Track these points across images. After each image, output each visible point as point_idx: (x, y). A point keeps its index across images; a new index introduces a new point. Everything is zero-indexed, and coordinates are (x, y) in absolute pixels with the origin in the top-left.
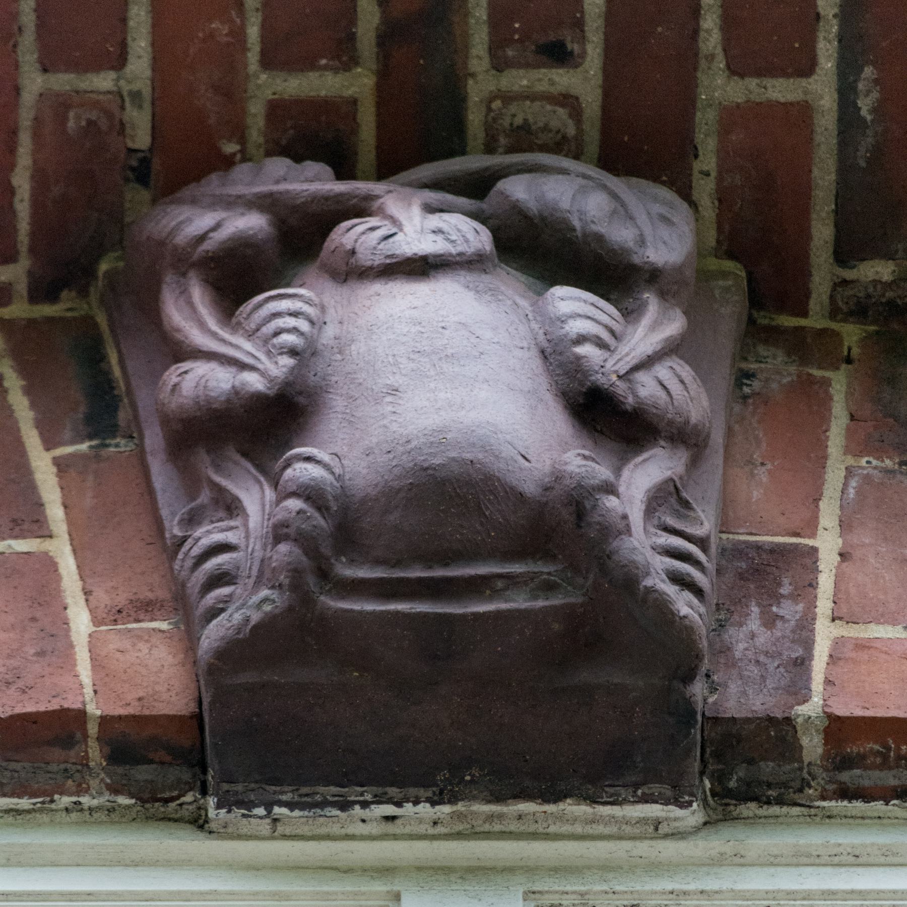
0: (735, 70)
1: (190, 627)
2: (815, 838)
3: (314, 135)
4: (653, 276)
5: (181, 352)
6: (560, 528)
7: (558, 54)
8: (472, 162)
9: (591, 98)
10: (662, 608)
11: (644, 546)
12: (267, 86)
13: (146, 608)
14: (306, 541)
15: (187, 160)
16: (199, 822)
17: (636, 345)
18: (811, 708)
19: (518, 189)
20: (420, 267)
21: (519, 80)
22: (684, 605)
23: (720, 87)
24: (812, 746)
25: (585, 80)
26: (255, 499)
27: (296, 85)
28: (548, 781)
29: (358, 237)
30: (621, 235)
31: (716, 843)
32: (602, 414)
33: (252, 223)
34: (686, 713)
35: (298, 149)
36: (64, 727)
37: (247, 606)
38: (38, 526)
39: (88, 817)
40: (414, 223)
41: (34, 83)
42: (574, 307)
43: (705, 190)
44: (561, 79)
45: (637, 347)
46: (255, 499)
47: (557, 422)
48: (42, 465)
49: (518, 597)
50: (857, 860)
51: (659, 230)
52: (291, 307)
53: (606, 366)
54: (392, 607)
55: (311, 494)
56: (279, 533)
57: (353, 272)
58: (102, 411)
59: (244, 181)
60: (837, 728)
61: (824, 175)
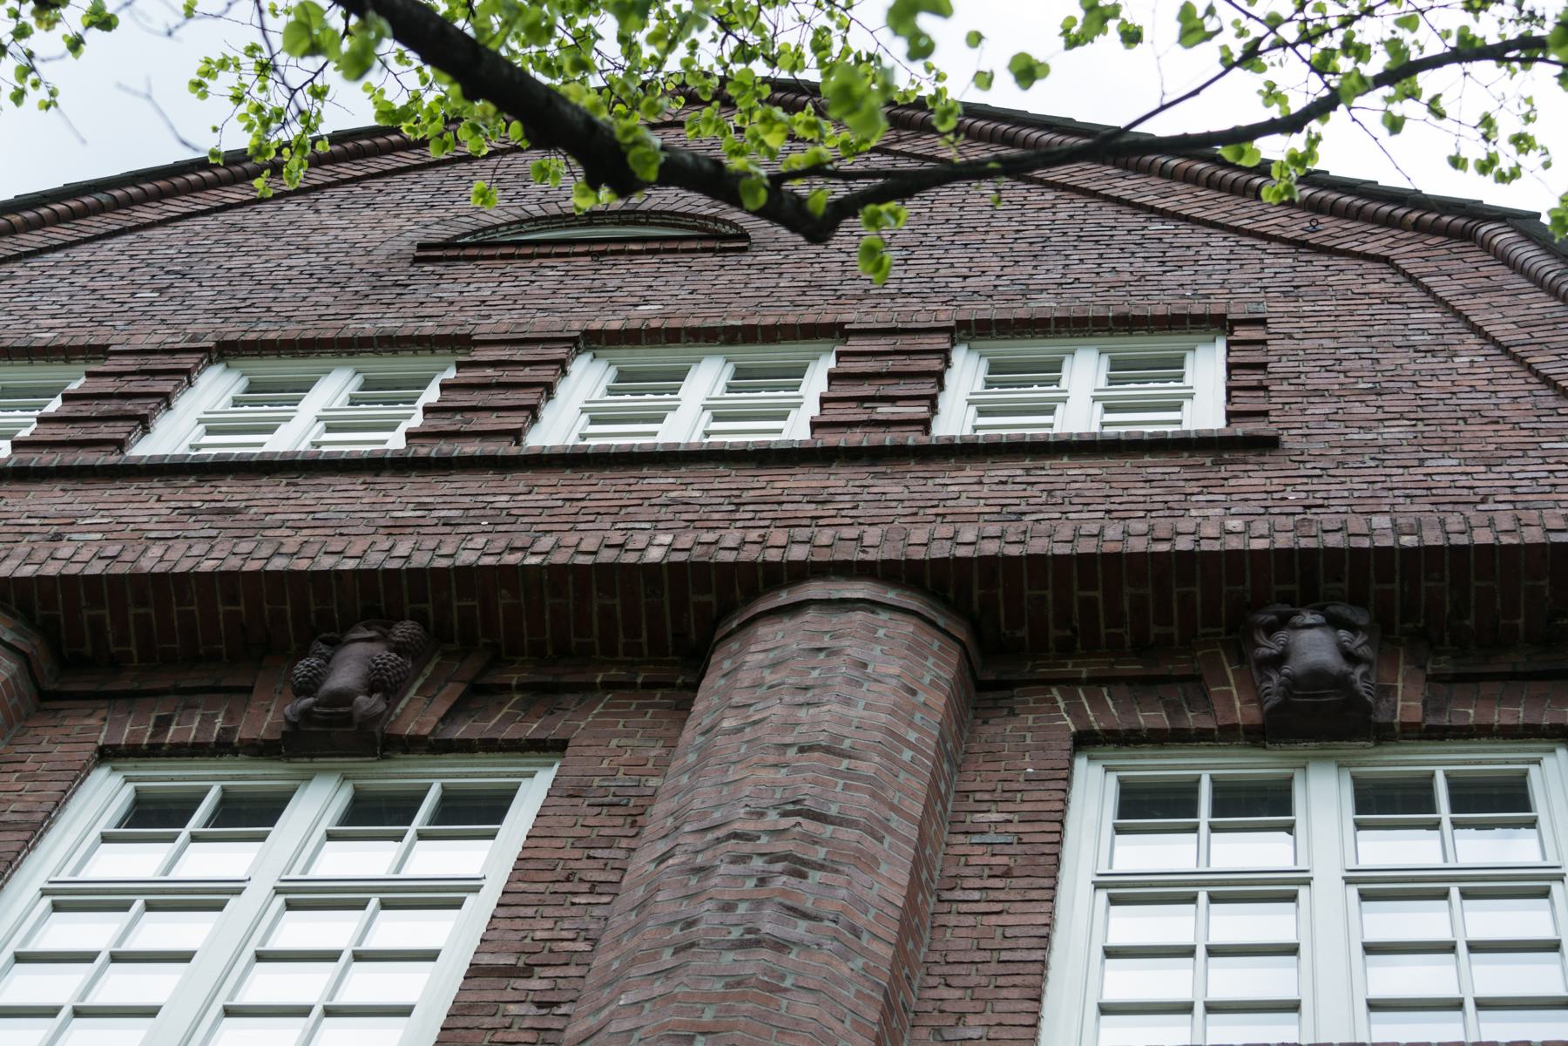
1: (1262, 704)
3: (1287, 599)
4: (1361, 627)
7: (1339, 580)
11: (1360, 686)
13: (1251, 701)
15: (1259, 604)
16: (1264, 747)
17: (1357, 643)
18: (1397, 720)
19: (1331, 609)
20: (1310, 626)
22: (1369, 698)
24: (1397, 729)
25: (1345, 585)
26: (1275, 677)
27: (1281, 588)
29: (1297, 620)
30: (1354, 618)
32: (1350, 657)
33: (1273, 617)
35: (1283, 602)
36: (1234, 727)
37: (1273, 701)
42: (1343, 634)
44: (1341, 585)
45: (1357, 643)
46: (1275, 677)
47: (1340, 659)
48: (1229, 671)
50: (1408, 753)
51: (1363, 619)
52: (1282, 636)
53: (1351, 647)
54: (1175, 606)
55: (1287, 675)
56: (1281, 684)
57: (1296, 628)
58: (1240, 658)
60: (1403, 724)
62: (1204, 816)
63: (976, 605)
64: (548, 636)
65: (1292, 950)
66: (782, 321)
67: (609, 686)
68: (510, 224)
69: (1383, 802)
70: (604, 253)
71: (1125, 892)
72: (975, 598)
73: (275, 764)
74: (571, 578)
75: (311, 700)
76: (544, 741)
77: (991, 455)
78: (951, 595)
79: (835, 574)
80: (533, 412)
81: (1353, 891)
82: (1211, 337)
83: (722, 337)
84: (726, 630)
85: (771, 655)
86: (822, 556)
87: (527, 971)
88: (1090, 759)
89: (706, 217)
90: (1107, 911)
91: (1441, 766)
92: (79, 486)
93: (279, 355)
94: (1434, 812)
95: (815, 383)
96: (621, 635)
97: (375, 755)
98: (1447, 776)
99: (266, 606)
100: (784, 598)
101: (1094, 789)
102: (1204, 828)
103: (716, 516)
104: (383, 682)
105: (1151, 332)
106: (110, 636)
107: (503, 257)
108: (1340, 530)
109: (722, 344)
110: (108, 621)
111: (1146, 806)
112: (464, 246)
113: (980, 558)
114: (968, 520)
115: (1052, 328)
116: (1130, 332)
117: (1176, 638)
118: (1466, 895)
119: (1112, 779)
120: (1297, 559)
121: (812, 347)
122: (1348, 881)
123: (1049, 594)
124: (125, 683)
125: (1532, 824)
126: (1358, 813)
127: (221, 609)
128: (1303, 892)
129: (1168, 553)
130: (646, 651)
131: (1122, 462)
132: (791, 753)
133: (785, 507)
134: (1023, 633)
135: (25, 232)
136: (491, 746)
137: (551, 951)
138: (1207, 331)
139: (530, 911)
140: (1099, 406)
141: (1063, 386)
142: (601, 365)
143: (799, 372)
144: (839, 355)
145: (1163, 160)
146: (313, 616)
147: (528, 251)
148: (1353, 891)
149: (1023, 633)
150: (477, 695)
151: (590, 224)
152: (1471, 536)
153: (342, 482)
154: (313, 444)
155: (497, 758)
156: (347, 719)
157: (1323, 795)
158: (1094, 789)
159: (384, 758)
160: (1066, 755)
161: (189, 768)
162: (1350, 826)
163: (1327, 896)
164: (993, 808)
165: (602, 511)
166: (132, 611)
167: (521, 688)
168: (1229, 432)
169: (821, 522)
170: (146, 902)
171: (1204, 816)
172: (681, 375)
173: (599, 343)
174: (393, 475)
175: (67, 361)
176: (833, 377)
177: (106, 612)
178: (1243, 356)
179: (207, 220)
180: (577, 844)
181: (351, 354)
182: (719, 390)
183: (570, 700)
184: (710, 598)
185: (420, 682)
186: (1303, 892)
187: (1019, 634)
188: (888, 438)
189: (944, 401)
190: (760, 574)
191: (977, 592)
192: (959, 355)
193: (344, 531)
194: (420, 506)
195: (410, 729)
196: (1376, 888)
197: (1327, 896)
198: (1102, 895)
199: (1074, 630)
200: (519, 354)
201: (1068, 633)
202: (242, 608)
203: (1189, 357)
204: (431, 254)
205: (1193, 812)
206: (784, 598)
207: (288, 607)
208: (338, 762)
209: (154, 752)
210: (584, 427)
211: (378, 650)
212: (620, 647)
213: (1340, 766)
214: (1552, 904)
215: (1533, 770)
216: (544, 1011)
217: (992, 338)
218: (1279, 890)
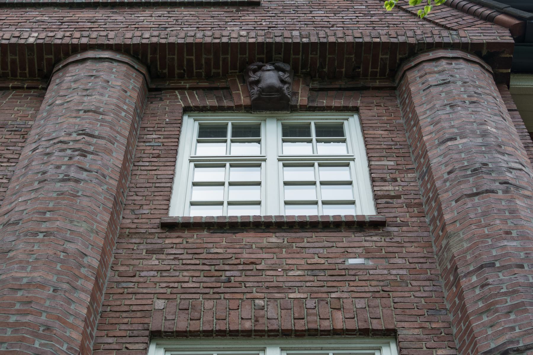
0: (294, 55)
2: (299, 114)
4: (287, 71)
5: (250, 77)
6: (279, 90)
7: (280, 54)
8: (273, 62)
9: (282, 57)
10: (287, 96)
11: (286, 92)
12: (257, 56)
13: (247, 97)
14: (259, 91)
15: (251, 62)
16: (251, 113)
17: (286, 76)
18: (299, 104)
19: (276, 64)
20: (269, 70)
21: (277, 56)
22: (289, 96)
23: (292, 56)
24: (298, 107)
25: (282, 56)
26: (256, 88)
27: (259, 56)
28: (278, 110)
29: (264, 68)
30: (284, 68)
31: (291, 114)
32: (283, 81)
33: (256, 67)
34: (289, 104)
36: (241, 106)
38: (239, 90)
39: (242, 113)
40: (269, 67)
41: (239, 56)
43: (291, 64)
44: (280, 56)
46: (256, 88)
47: (279, 82)
48: (239, 86)
49: (276, 96)
50: (302, 116)
51: (288, 68)
52: (259, 73)
53: (283, 78)
55: (260, 88)
56: (258, 91)
57: (264, 71)
58: (244, 81)
59: (255, 64)
60: (300, 106)
61: (300, 63)
62: (229, 137)
63: (149, 61)
67: (14, 88)
69: (292, 133)
71: (200, 163)
72: (149, 58)
78: (140, 57)
79: (98, 48)
81: (281, 163)
86: (93, 42)
88: (189, 116)
90: (194, 170)
91: (313, 120)
96: (19, 70)
98: (315, 124)
100: (79, 57)
101: (190, 127)
110: (194, 61)
111: (208, 133)
119: (197, 124)
122: (279, 160)
123: (176, 57)
125: (344, 141)
128: (263, 164)
130: (28, 75)
132: (81, 113)
134: (166, 71)
148: (281, 163)
149: (166, 71)
157: (271, 131)
158: (190, 127)
163: (272, 166)
164: (154, 133)
171: (229, 137)
186: (263, 164)
190: (70, 48)
191: (149, 56)
196: (289, 163)
197: (272, 166)
198: (192, 164)
199: (184, 70)
201: (182, 71)
206: (79, 57)
212: (18, 74)
213: (278, 120)
215: (346, 122)
218: (255, 163)
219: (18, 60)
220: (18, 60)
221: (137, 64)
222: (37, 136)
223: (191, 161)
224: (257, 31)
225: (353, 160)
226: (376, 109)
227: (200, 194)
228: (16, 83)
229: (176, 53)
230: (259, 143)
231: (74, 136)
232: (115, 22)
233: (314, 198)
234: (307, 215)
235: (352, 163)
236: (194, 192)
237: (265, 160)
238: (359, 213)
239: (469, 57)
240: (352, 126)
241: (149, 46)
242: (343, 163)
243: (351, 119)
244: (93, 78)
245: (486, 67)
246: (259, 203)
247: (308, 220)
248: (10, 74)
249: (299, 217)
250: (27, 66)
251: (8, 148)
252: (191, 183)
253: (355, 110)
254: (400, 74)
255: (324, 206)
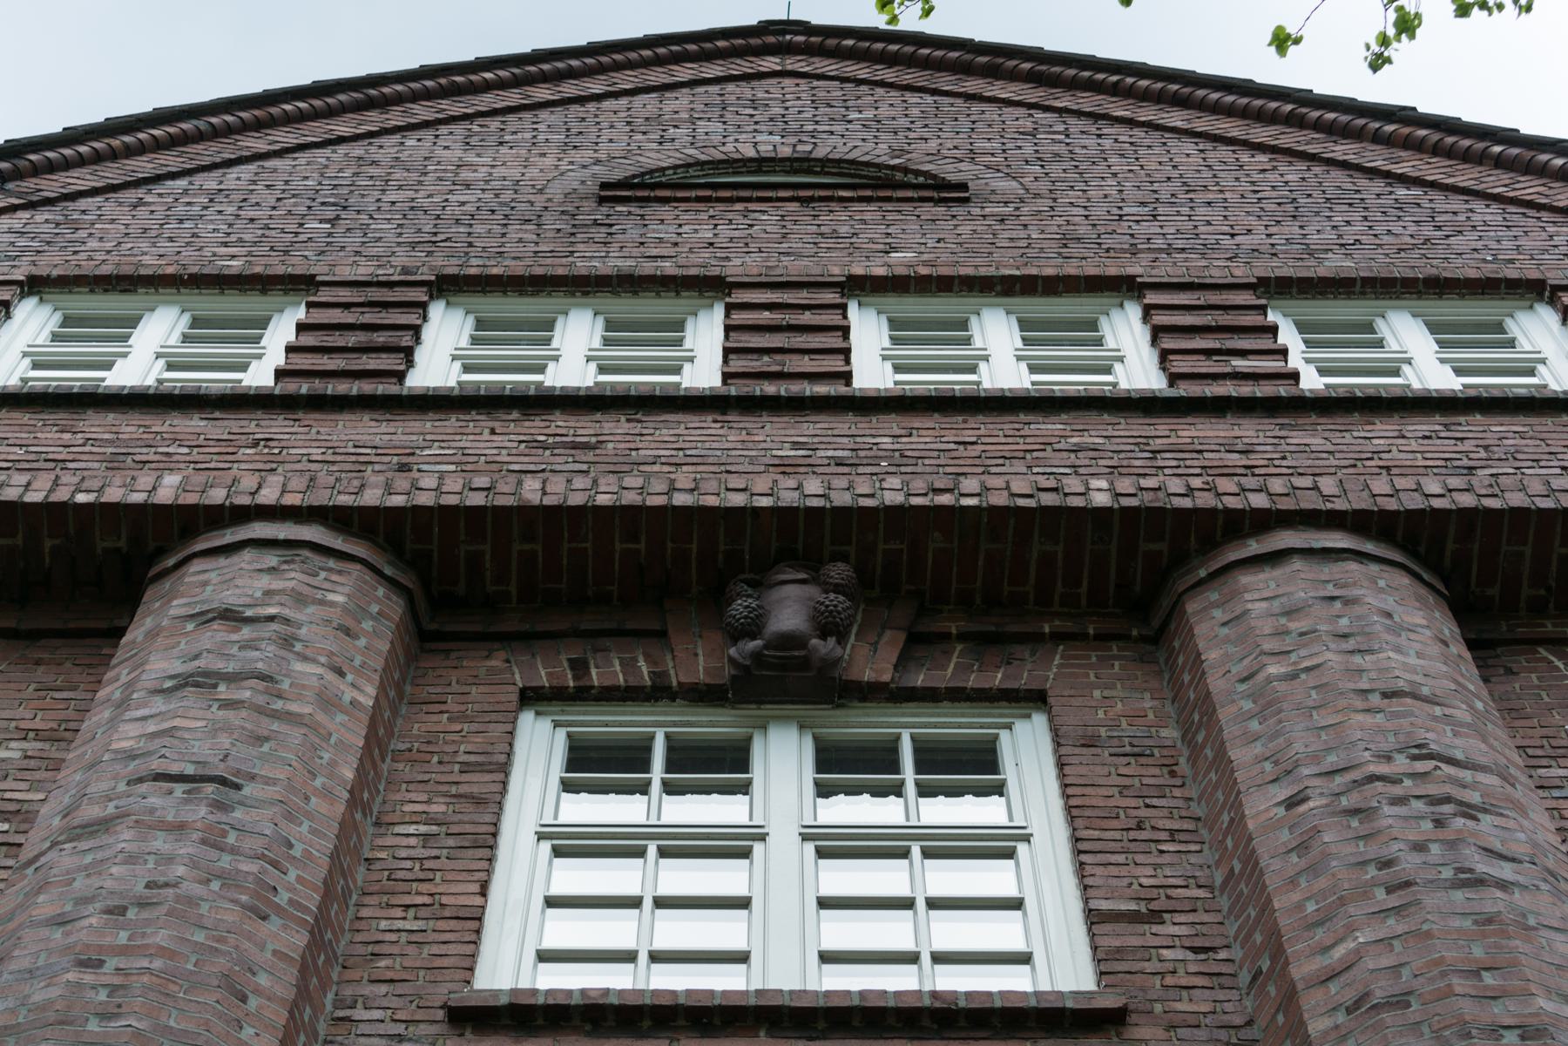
62: (657, 772)
63: (1447, 561)
64: (979, 583)
65: (743, 903)
66: (160, 272)
67: (1058, 637)
68: (676, 167)
69: (841, 765)
70: (812, 199)
71: (570, 844)
72: (1448, 553)
73: (719, 710)
74: (1012, 522)
75: (758, 643)
76: (1017, 691)
77: (1396, 410)
78: (1422, 549)
79: (1301, 523)
80: (408, 354)
81: (810, 848)
82: (708, 301)
83: (999, 288)
84: (1190, 580)
85: (1276, 603)
86: (1285, 504)
87: (1155, 917)
88: (538, 714)
89: (893, 168)
90: (657, 863)
91: (906, 730)
92: (388, 416)
93: (505, 293)
94: (747, 772)
95: (281, 332)
96: (1059, 584)
97: (832, 702)
98: (913, 738)
99: (670, 545)
100: (1254, 547)
101: (539, 745)
102: (656, 787)
103: (1137, 463)
104: (837, 625)
105: (1462, 296)
106: (488, 573)
107: (699, 199)
108: (692, 490)
109: (998, 295)
110: (488, 557)
111: (595, 764)
112: (653, 186)
113: (519, 507)
114: (444, 471)
115: (1358, 288)
116: (1440, 295)
117: (1032, 596)
118: (663, 853)
119: (561, 734)
120: (828, 521)
121: (1098, 301)
122: (805, 838)
123: (1528, 550)
124: (511, 625)
125: (998, 789)
126: (667, 772)
127: (618, 546)
128: (758, 848)
129: (456, 507)
130: (1084, 602)
131: (1543, 420)
132: (1375, 699)
133: (1206, 455)
134: (1494, 591)
135: (127, 157)
136: (957, 695)
137: (1168, 897)
138: (1522, 297)
139: (1121, 858)
140: (458, 365)
141: (555, 344)
142: (47, 310)
143: (263, 323)
144: (310, 305)
145: (1377, 125)
146: (721, 557)
147: (727, 194)
148: (810, 848)
149: (1494, 591)
150: (919, 643)
151: (758, 172)
152: (670, 498)
153: (693, 420)
154: (22, 379)
155: (964, 707)
156: (805, 663)
157: (783, 758)
158: (539, 745)
159: (839, 706)
160: (513, 706)
161: (624, 714)
162: (554, 783)
163: (784, 850)
164: (1553, 763)
165: (1008, 455)
166: (517, 547)
167: (963, 637)
168: (724, 391)
169: (1257, 471)
170: (659, 848)
171: (657, 772)
172: (133, 322)
173: (863, 290)
174: (741, 414)
175: (264, 292)
176: (301, 328)
177: (487, 548)
178: (739, 317)
179: (327, 152)
180: (1125, 792)
181: (586, 294)
182: (175, 339)
183: (1023, 651)
184: (1162, 546)
185: (854, 630)
186: (758, 848)
187: (1490, 592)
188: (1246, 390)
189: (420, 355)
190: (1220, 522)
191: (1450, 546)
192: (437, 310)
193: (729, 468)
194: (796, 445)
195: (868, 676)
196: (833, 846)
197: (784, 850)
198: (546, 846)
199: (1549, 589)
200: (801, 297)
201: (1543, 592)
202: (642, 546)
203: (974, 320)
204: (614, 192)
205: (645, 767)
206: (1254, 547)
207: (694, 546)
208: (790, 709)
209: (582, 695)
210: (25, 371)
211: (812, 591)
212: (1057, 598)
213: (802, 727)
214: (1017, 865)
215: (1004, 735)
216: (1202, 956)
217: (1292, 298)
218: (734, 845)
219: (1060, 555)
220: (1060, 555)
221: (390, 563)
222: (1268, 766)
223: (541, 837)
224: (1033, 478)
225: (1027, 839)
226: (1116, 698)
227: (568, 930)
228: (1068, 626)
229: (1531, 538)
230: (1001, 795)
231: (1401, 763)
232: (1304, 449)
233: (907, 945)
234: (994, 989)
235: (1022, 848)
236: (548, 924)
237: (762, 838)
238: (1045, 986)
239: (1369, 547)
240: (1027, 748)
241: (882, 514)
242: (996, 846)
243: (1020, 726)
244: (1338, 605)
245: (1425, 576)
246: (742, 958)
247: (962, 1004)
248: (1032, 596)
249: (689, 992)
250: (1086, 574)
251: (1148, 801)
252: (541, 900)
253: (1036, 699)
254: (1166, 603)
255: (825, 967)
